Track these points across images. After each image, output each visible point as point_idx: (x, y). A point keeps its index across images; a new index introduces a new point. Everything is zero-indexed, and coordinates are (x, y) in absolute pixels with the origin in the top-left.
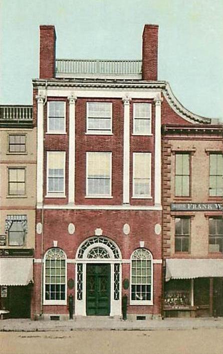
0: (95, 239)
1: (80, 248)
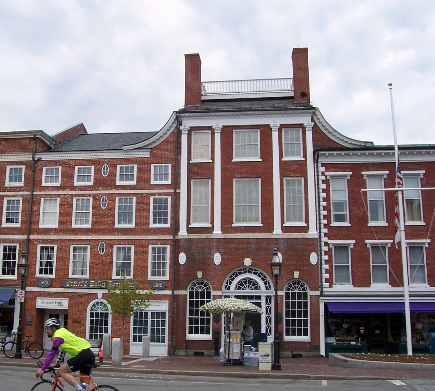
0: (244, 270)
1: (227, 279)
